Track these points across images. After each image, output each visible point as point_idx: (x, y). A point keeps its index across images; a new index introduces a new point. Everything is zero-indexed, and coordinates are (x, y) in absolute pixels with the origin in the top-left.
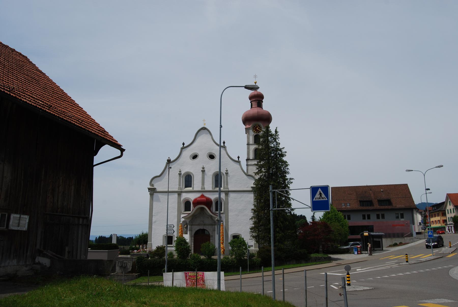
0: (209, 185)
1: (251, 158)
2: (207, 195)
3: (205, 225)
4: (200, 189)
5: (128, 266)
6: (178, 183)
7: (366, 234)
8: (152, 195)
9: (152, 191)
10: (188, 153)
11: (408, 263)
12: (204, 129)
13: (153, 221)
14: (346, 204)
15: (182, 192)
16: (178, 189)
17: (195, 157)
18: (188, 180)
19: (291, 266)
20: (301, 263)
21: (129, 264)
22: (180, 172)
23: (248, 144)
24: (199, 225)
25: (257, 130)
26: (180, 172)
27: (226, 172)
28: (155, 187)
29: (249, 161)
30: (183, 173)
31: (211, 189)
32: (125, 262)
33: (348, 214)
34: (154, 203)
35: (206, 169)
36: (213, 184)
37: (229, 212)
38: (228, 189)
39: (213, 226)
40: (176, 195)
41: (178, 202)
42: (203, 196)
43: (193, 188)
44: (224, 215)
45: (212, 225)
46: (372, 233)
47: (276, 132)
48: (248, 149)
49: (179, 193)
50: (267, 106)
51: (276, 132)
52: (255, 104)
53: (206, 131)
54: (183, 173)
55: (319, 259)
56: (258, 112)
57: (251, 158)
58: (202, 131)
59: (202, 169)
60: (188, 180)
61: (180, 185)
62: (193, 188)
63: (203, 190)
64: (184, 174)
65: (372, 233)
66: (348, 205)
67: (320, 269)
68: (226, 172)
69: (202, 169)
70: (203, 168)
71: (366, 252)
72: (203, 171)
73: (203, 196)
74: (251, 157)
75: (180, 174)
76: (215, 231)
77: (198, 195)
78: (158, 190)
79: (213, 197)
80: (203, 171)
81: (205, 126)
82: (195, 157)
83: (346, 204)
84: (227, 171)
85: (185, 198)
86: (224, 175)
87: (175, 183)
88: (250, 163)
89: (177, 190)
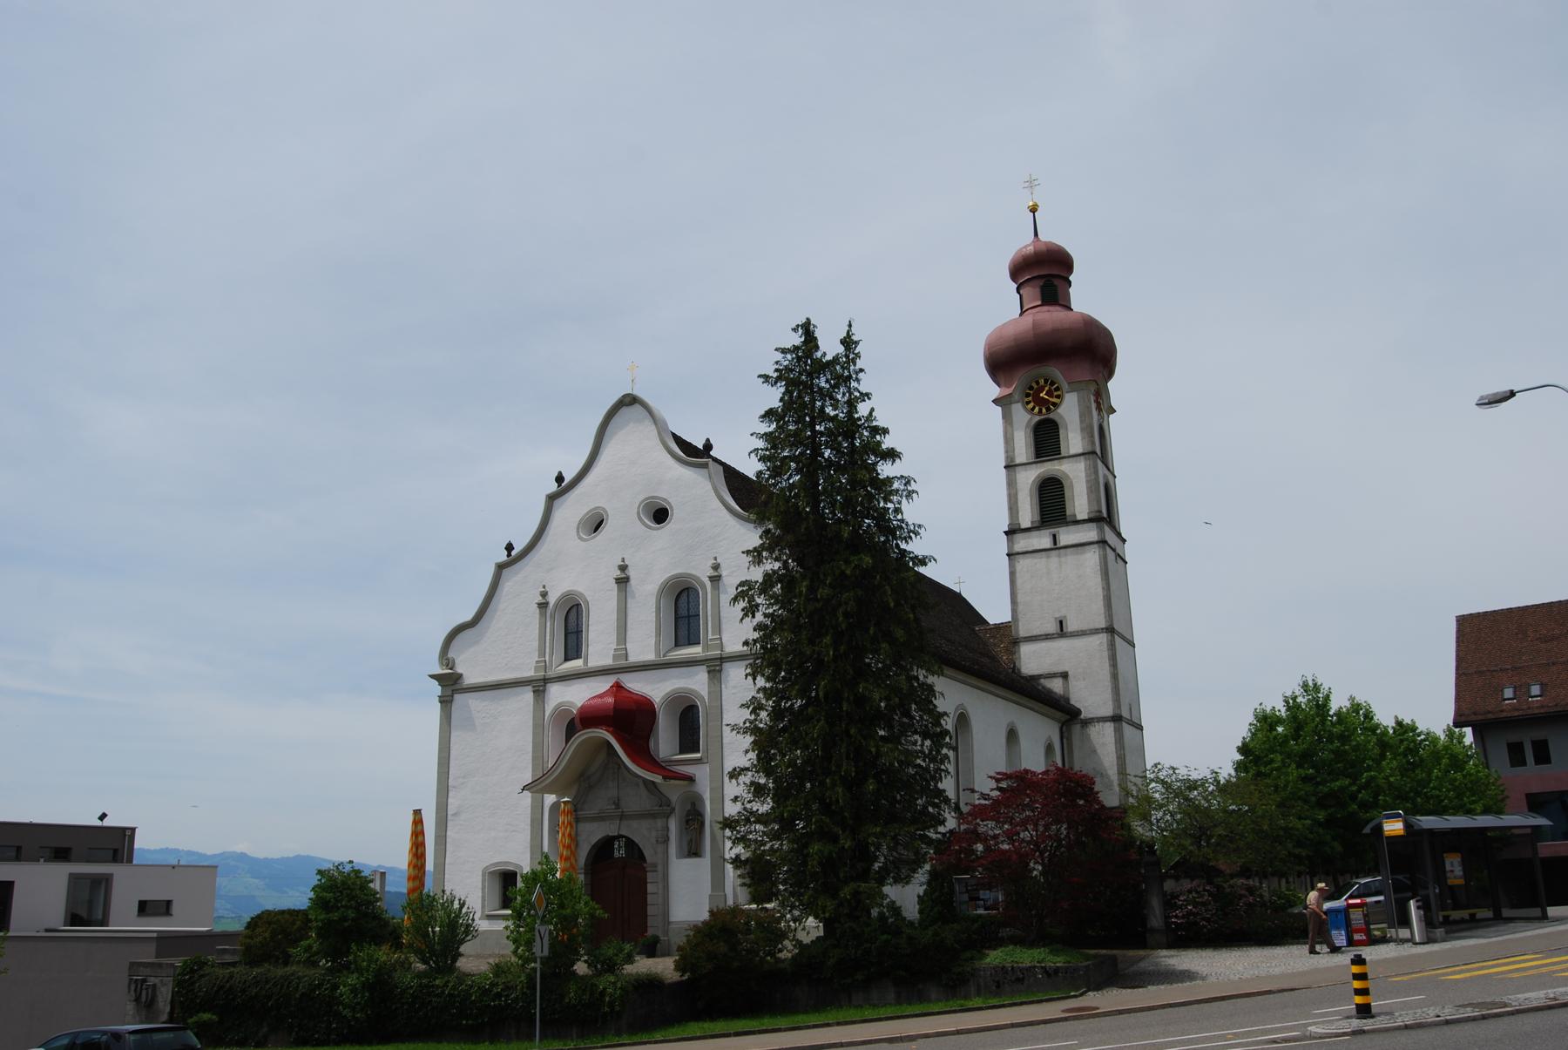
0: (644, 645)
1: (1026, 522)
2: (638, 685)
3: (622, 817)
4: (608, 661)
5: (160, 999)
6: (536, 644)
7: (1394, 827)
8: (446, 701)
9: (451, 684)
10: (571, 511)
11: (1367, 1024)
12: (629, 401)
13: (450, 812)
14: (1521, 690)
15: (546, 681)
16: (536, 669)
17: (596, 524)
18: (570, 622)
19: (852, 1014)
20: (922, 998)
21: (164, 990)
22: (544, 595)
23: (1010, 467)
24: (600, 818)
25: (1040, 402)
26: (544, 595)
27: (711, 572)
28: (459, 670)
29: (1018, 536)
30: (552, 599)
31: (650, 656)
32: (152, 981)
33: (1539, 734)
34: (456, 736)
35: (631, 572)
36: (658, 634)
37: (726, 752)
38: (721, 647)
39: (660, 823)
40: (527, 695)
41: (535, 726)
42: (618, 687)
43: (586, 662)
44: (707, 768)
45: (652, 816)
46: (1427, 822)
47: (848, 342)
48: (1011, 484)
49: (540, 686)
50: (1087, 297)
51: (848, 342)
52: (1031, 292)
53: (637, 407)
54: (552, 599)
55: (1020, 980)
56: (1035, 324)
57: (1026, 522)
58: (624, 410)
59: (618, 573)
60: (570, 622)
61: (542, 653)
62: (586, 662)
63: (622, 663)
64: (556, 605)
65: (1427, 822)
66: (1535, 690)
67: (901, 1039)
68: (711, 572)
69: (618, 573)
70: (623, 568)
71: (1404, 933)
72: (623, 581)
73: (618, 687)
74: (1027, 517)
75: (543, 606)
76: (666, 840)
77: (602, 685)
78: (471, 677)
79: (655, 688)
80: (623, 581)
81: (636, 393)
82: (596, 524)
83: (1521, 690)
84: (716, 567)
85: (560, 705)
86: (703, 586)
87: (512, 645)
88: (1022, 543)
89: (529, 673)
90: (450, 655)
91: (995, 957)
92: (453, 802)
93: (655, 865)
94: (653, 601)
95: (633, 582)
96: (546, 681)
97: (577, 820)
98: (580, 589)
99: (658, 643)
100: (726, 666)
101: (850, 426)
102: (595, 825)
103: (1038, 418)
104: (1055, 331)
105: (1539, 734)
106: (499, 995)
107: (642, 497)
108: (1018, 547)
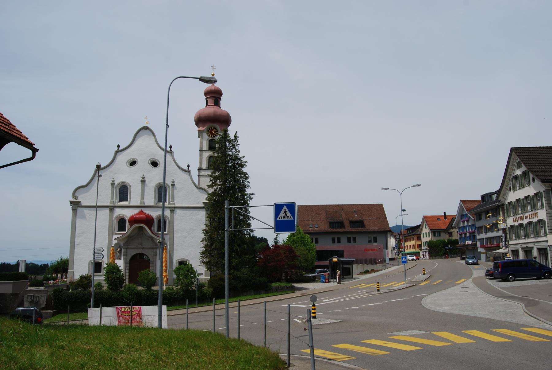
1: (204, 167)
2: (148, 212)
3: (143, 248)
6: (110, 196)
9: (76, 205)
12: (146, 128)
14: (313, 226)
17: (133, 163)
18: (123, 192)
19: (249, 297)
20: (260, 293)
21: (43, 298)
22: (113, 181)
23: (201, 150)
24: (136, 248)
25: (212, 134)
26: (113, 181)
27: (172, 183)
29: (201, 171)
30: (116, 183)
31: (152, 204)
32: (37, 295)
34: (78, 221)
35: (146, 179)
38: (174, 204)
40: (107, 211)
41: (109, 220)
44: (169, 236)
45: (153, 248)
46: (342, 259)
47: (236, 137)
48: (201, 156)
49: (112, 209)
50: (225, 105)
51: (236, 137)
52: (211, 101)
53: (148, 131)
54: (116, 183)
56: (214, 112)
57: (204, 167)
58: (143, 130)
61: (112, 198)
62: (130, 203)
63: (143, 205)
64: (118, 185)
65: (342, 259)
68: (172, 183)
72: (143, 182)
73: (142, 212)
74: (205, 166)
75: (113, 185)
76: (156, 255)
77: (136, 211)
79: (155, 214)
80: (143, 182)
81: (147, 125)
82: (133, 163)
83: (313, 226)
84: (173, 182)
85: (119, 215)
86: (169, 187)
88: (203, 173)
89: (108, 204)
90: (76, 195)
91: (274, 285)
92: (77, 241)
93: (153, 262)
94: (153, 189)
95: (147, 182)
96: (114, 207)
97: (127, 249)
98: (128, 181)
99: (155, 201)
100: (176, 209)
101: (236, 158)
102: (133, 250)
103: (211, 138)
104: (220, 115)
105: (317, 237)
106: (175, 295)
107: (150, 158)
108: (201, 174)
